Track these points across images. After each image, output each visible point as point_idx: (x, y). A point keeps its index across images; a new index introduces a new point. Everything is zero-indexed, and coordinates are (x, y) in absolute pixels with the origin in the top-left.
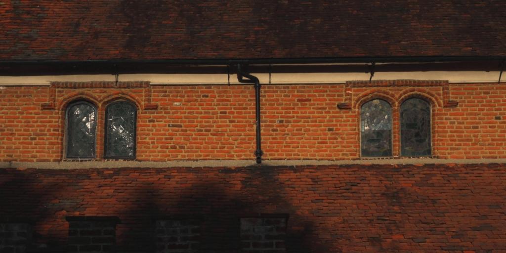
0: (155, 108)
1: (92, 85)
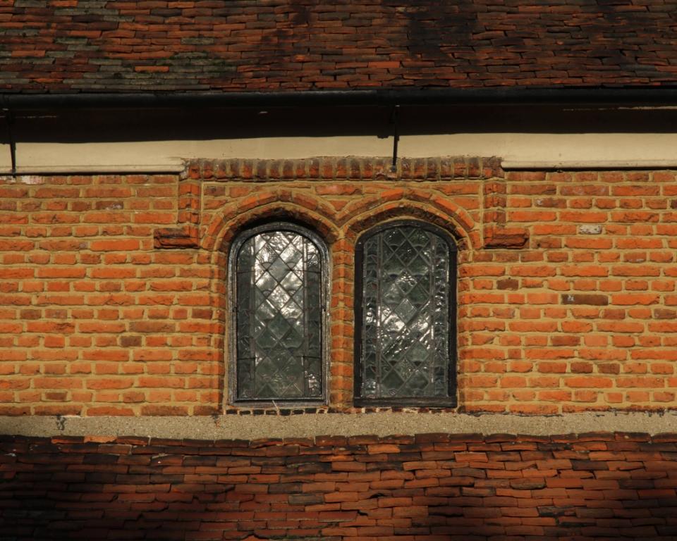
0: (519, 242)
1: (315, 172)
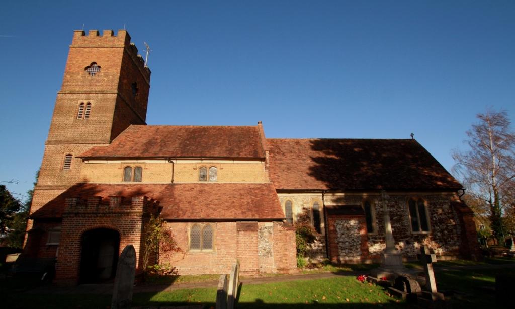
0: (147, 169)
1: (131, 163)
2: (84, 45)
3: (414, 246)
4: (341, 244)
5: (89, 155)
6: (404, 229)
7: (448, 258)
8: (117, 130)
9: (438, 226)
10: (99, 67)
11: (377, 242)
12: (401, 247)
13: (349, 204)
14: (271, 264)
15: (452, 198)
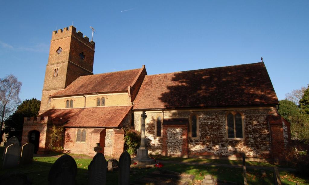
2: (56, 39)
3: (227, 149)
4: (169, 144)
5: (54, 96)
6: (221, 135)
7: (258, 160)
8: (68, 82)
9: (252, 135)
10: (62, 49)
11: (198, 144)
12: (216, 148)
13: (181, 118)
14: (111, 152)
15: (270, 112)
